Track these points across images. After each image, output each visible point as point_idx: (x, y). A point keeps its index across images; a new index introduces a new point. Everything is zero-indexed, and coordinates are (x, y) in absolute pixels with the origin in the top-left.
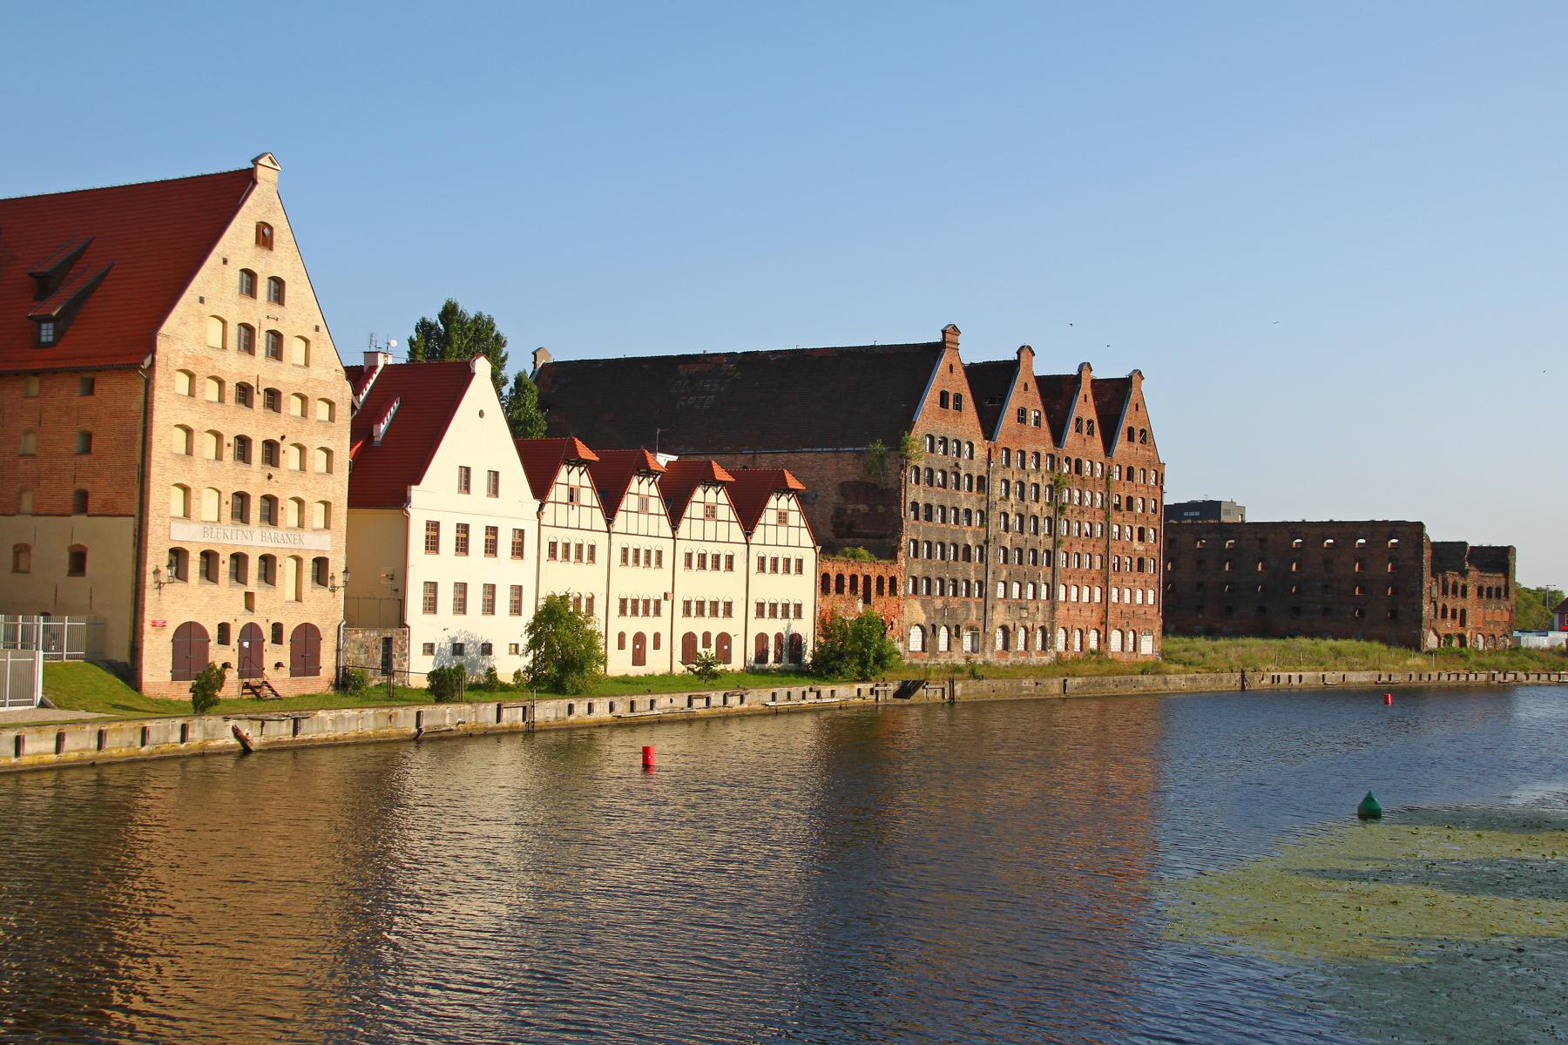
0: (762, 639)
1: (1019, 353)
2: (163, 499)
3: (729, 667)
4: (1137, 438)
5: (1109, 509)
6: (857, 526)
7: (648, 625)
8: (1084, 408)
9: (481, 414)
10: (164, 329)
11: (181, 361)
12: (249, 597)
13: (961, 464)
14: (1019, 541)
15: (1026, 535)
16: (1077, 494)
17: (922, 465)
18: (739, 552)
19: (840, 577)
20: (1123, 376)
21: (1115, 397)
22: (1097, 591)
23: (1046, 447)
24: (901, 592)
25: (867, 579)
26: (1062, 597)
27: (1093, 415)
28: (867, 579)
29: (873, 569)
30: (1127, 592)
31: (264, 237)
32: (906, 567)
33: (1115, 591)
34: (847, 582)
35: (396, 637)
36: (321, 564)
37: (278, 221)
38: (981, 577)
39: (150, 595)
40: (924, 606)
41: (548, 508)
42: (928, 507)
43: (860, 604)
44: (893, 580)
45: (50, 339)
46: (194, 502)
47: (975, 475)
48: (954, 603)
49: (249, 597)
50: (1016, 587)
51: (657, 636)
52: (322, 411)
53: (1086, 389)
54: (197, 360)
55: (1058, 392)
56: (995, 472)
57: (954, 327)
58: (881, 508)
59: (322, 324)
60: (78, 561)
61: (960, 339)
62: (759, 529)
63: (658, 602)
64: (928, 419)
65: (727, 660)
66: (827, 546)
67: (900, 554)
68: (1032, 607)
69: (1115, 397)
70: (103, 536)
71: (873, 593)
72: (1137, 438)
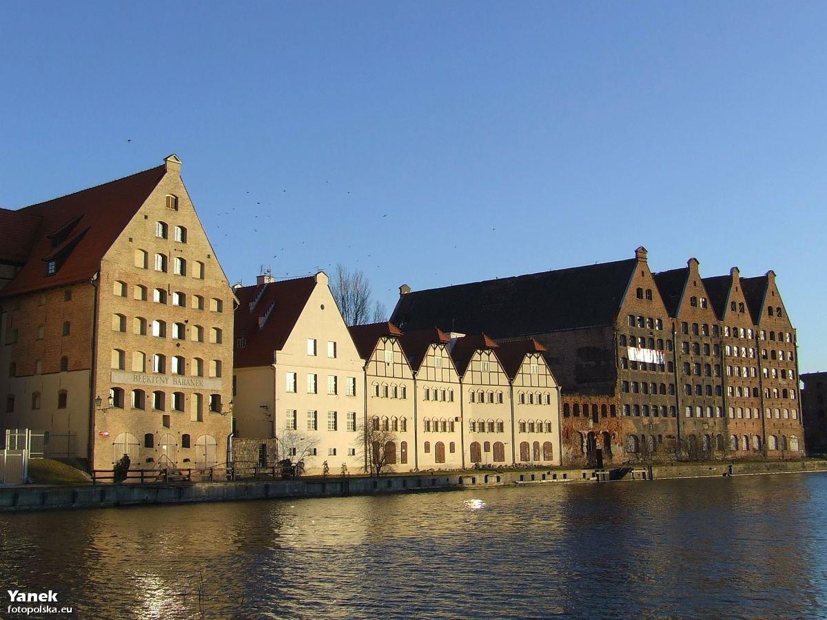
0: (524, 446)
1: (688, 263)
2: (108, 358)
3: (503, 464)
4: (775, 313)
5: (759, 359)
6: (588, 379)
7: (446, 438)
8: (736, 295)
9: (322, 307)
10: (105, 257)
11: (117, 276)
12: (166, 418)
13: (655, 333)
14: (699, 380)
15: (703, 376)
16: (735, 349)
17: (628, 334)
18: (410, 385)
19: (576, 406)
20: (762, 274)
21: (758, 292)
22: (756, 412)
23: (712, 320)
24: (619, 414)
25: (595, 407)
26: (731, 415)
27: (743, 300)
28: (595, 407)
29: (599, 401)
30: (777, 411)
31: (175, 204)
32: (621, 399)
33: (768, 411)
34: (581, 408)
35: (268, 444)
36: (216, 398)
37: (182, 194)
38: (674, 404)
39: (98, 416)
40: (636, 423)
41: (372, 364)
42: (663, 385)
43: (591, 423)
44: (613, 407)
45: (53, 271)
46: (127, 360)
47: (665, 339)
48: (656, 420)
49: (166, 418)
50: (698, 410)
51: (452, 446)
52: (213, 306)
53: (736, 283)
54: (128, 275)
55: (718, 288)
56: (678, 337)
57: (643, 249)
58: (603, 363)
59: (211, 253)
60: (63, 399)
61: (648, 255)
62: (519, 377)
63: (452, 423)
64: (630, 304)
65: (550, 458)
66: (566, 389)
67: (617, 390)
68: (711, 422)
69: (758, 292)
70: (74, 381)
71: (600, 416)
72: (775, 313)
